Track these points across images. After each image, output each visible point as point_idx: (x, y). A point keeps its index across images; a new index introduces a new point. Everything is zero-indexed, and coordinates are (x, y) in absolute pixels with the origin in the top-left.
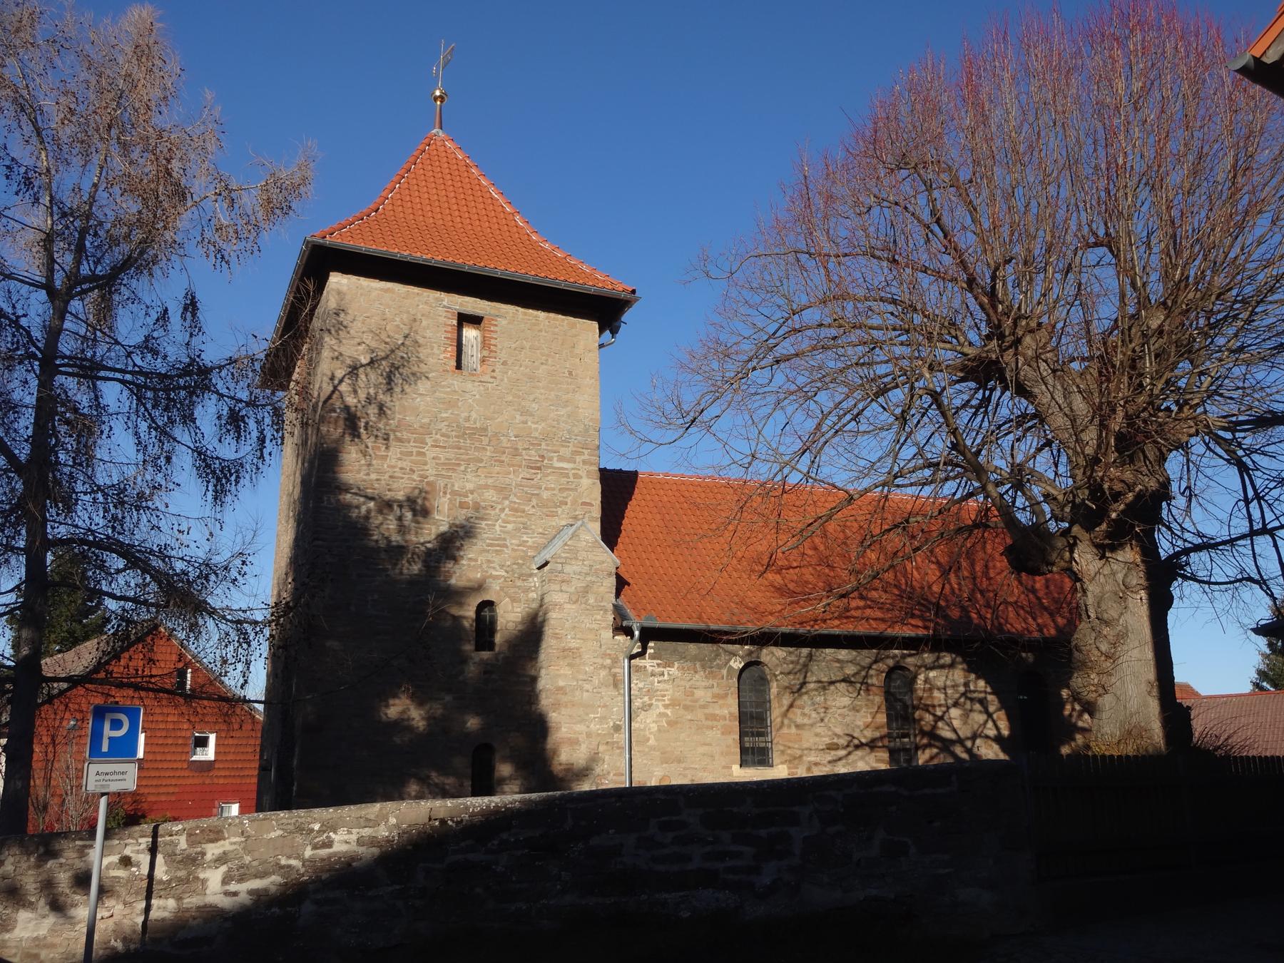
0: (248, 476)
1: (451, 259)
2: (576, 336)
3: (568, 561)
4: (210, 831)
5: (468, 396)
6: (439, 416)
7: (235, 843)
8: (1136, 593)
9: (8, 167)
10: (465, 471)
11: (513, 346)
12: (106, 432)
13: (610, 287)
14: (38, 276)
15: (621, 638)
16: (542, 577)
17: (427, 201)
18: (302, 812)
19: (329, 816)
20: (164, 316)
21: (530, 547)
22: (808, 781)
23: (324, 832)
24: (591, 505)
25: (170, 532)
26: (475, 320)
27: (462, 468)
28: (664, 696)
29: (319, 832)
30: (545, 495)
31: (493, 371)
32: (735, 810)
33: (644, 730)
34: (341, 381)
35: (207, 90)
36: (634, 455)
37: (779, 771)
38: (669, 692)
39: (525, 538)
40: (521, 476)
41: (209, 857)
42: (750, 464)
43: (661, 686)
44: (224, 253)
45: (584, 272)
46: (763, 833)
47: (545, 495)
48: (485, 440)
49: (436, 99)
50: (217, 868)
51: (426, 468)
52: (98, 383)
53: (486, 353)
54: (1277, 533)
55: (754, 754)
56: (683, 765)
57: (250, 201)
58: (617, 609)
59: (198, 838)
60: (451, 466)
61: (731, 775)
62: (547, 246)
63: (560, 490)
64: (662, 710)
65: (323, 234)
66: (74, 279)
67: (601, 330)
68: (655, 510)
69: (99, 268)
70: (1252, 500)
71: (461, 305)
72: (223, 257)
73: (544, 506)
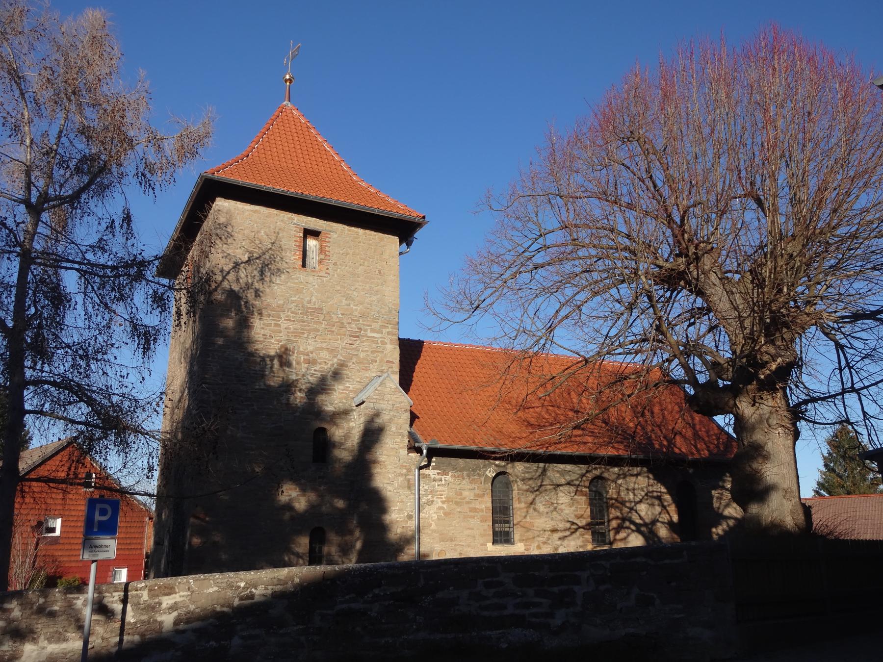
0: (162, 338)
1: (300, 191)
2: (384, 246)
3: (378, 401)
4: (165, 587)
5: (309, 286)
6: (290, 299)
7: (183, 596)
8: (776, 429)
9: (4, 118)
10: (307, 338)
11: (341, 252)
12: (73, 305)
13: (408, 214)
14: (20, 194)
15: (414, 455)
16: (359, 412)
17: (281, 151)
18: (232, 574)
19: (251, 577)
20: (111, 227)
21: (351, 391)
22: (586, 554)
23: (248, 588)
24: (393, 363)
25: (114, 376)
26: (315, 234)
27: (305, 335)
28: (442, 495)
29: (244, 588)
30: (362, 355)
31: (327, 269)
32: (537, 574)
33: (428, 518)
34: (228, 273)
35: (141, 70)
36: (436, 329)
37: (517, 549)
38: (445, 492)
39: (348, 385)
40: (346, 342)
41: (164, 605)
42: (516, 337)
43: (440, 488)
44: (151, 182)
45: (390, 203)
46: (556, 589)
47: (362, 355)
48: (321, 316)
49: (286, 81)
50: (170, 613)
51: (281, 335)
52: (59, 270)
53: (322, 257)
54: (861, 392)
55: (501, 537)
56: (454, 543)
57: (169, 147)
58: (410, 434)
59: (156, 593)
60: (298, 334)
61: (486, 550)
62: (364, 184)
63: (372, 352)
64: (440, 504)
65: (213, 171)
66: (44, 197)
67: (401, 243)
68: (433, 367)
69: (63, 191)
70: (845, 368)
71: (306, 223)
72: (150, 185)
73: (361, 363)
